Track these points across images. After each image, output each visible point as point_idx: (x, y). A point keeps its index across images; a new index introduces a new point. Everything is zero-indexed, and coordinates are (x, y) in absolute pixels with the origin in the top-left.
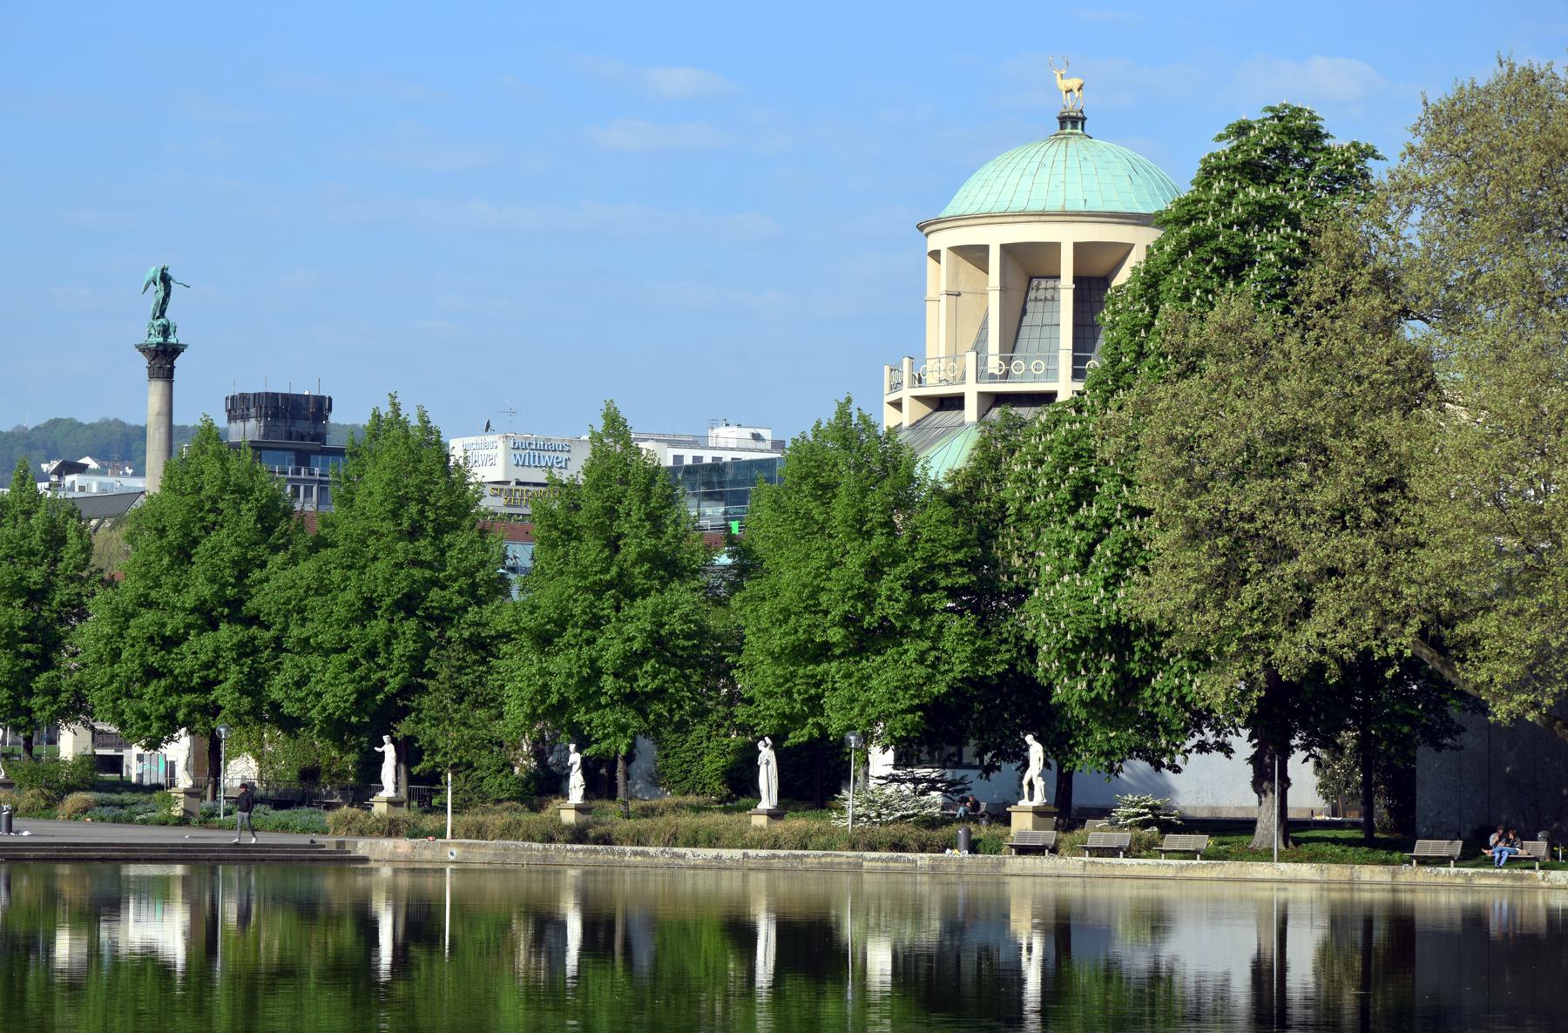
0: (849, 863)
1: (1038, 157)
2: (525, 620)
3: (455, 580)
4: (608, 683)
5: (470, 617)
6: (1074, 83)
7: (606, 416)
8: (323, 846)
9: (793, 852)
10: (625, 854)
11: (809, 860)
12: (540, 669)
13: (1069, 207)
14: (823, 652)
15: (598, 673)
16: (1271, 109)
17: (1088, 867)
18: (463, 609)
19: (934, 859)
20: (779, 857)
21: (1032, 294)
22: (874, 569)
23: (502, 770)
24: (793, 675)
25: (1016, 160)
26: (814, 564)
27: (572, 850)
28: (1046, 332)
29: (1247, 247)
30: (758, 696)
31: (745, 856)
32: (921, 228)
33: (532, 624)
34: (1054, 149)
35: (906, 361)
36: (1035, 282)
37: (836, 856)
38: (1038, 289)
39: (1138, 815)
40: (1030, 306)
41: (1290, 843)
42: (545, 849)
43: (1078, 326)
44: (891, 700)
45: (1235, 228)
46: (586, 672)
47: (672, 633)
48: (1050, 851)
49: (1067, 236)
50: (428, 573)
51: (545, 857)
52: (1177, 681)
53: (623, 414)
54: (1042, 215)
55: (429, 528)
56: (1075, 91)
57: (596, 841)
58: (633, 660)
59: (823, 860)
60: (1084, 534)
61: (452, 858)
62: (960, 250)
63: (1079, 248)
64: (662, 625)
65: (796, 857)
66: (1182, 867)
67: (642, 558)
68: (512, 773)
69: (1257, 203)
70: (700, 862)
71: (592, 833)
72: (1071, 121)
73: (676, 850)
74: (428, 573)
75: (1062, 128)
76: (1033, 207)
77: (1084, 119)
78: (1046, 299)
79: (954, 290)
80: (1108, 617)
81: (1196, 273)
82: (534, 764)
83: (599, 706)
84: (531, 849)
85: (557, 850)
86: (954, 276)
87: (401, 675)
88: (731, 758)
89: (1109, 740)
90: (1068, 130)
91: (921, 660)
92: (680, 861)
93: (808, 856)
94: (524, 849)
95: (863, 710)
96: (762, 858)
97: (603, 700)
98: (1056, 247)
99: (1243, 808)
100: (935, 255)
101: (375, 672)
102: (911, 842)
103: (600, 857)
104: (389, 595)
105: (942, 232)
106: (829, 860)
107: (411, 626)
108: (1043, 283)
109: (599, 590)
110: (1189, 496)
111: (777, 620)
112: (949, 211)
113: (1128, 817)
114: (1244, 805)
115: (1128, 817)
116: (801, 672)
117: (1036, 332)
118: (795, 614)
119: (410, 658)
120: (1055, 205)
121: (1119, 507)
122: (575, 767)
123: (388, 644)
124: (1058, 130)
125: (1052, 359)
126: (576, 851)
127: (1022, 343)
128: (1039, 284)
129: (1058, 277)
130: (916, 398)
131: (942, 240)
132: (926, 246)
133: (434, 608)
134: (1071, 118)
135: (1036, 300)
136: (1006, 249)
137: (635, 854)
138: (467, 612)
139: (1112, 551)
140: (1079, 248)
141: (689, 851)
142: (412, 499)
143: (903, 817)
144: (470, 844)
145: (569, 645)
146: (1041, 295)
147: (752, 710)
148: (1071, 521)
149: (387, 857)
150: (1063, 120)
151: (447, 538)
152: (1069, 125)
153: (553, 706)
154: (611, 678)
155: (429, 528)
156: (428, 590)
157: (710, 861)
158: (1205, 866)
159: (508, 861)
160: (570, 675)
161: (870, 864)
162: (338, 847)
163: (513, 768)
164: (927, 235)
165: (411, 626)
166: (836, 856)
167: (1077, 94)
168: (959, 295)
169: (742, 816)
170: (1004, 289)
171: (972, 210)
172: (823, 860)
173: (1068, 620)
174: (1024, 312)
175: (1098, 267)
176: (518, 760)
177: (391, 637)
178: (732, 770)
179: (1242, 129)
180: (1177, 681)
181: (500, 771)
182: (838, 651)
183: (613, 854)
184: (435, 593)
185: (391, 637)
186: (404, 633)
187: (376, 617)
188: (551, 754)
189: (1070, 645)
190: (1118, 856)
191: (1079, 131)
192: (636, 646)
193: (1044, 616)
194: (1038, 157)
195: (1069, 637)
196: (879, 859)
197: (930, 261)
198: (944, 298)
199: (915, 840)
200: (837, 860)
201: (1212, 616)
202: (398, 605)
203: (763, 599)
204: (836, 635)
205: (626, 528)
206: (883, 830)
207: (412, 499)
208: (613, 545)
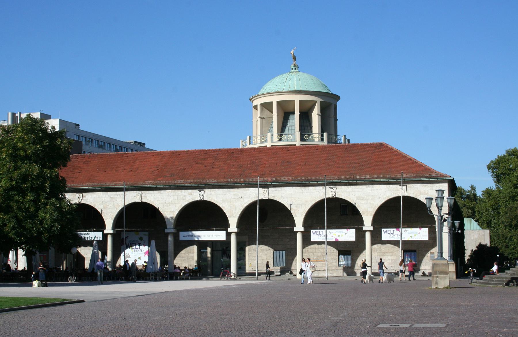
54: (289, 92)
62: (263, 105)
100: (256, 107)
112: (261, 92)
131: (258, 102)
136: (278, 103)
197: (254, 110)
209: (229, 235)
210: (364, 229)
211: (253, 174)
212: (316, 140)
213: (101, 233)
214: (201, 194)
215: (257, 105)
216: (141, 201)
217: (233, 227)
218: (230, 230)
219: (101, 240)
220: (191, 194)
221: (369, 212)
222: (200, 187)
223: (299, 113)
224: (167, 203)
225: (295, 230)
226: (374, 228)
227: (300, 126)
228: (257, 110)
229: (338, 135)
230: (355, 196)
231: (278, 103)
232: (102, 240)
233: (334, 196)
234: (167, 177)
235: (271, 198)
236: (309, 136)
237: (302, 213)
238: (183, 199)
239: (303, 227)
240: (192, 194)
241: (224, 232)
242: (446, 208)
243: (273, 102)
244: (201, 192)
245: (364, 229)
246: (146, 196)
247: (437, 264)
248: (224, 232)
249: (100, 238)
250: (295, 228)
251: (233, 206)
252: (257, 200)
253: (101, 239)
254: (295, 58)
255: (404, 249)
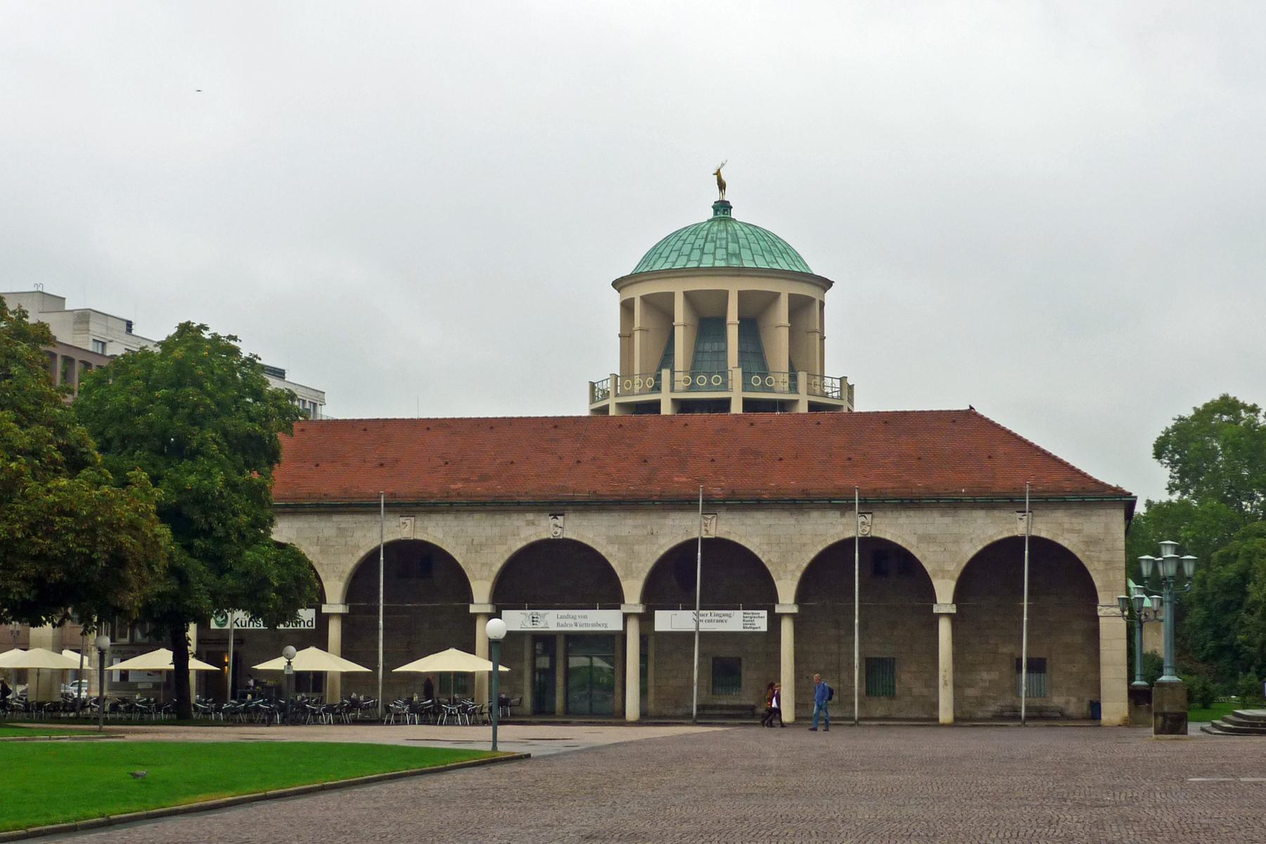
136: (687, 295)
209: (775, 620)
210: (935, 611)
211: (676, 479)
213: (313, 611)
214: (558, 524)
215: (634, 298)
216: (412, 539)
217: (787, 601)
218: (778, 610)
219: (311, 628)
220: (533, 524)
221: (949, 571)
222: (556, 507)
223: (738, 322)
224: (474, 543)
225: (471, 611)
226: (958, 609)
229: (825, 375)
230: (915, 534)
231: (642, 298)
232: (314, 627)
233: (867, 534)
234: (472, 481)
235: (722, 536)
237: (794, 571)
238: (515, 535)
239: (795, 603)
240: (536, 522)
241: (764, 613)
242: (1121, 565)
244: (557, 519)
245: (935, 611)
246: (425, 525)
248: (764, 613)
249: (310, 624)
250: (776, 606)
251: (633, 552)
252: (697, 539)
253: (312, 626)
254: (722, 186)
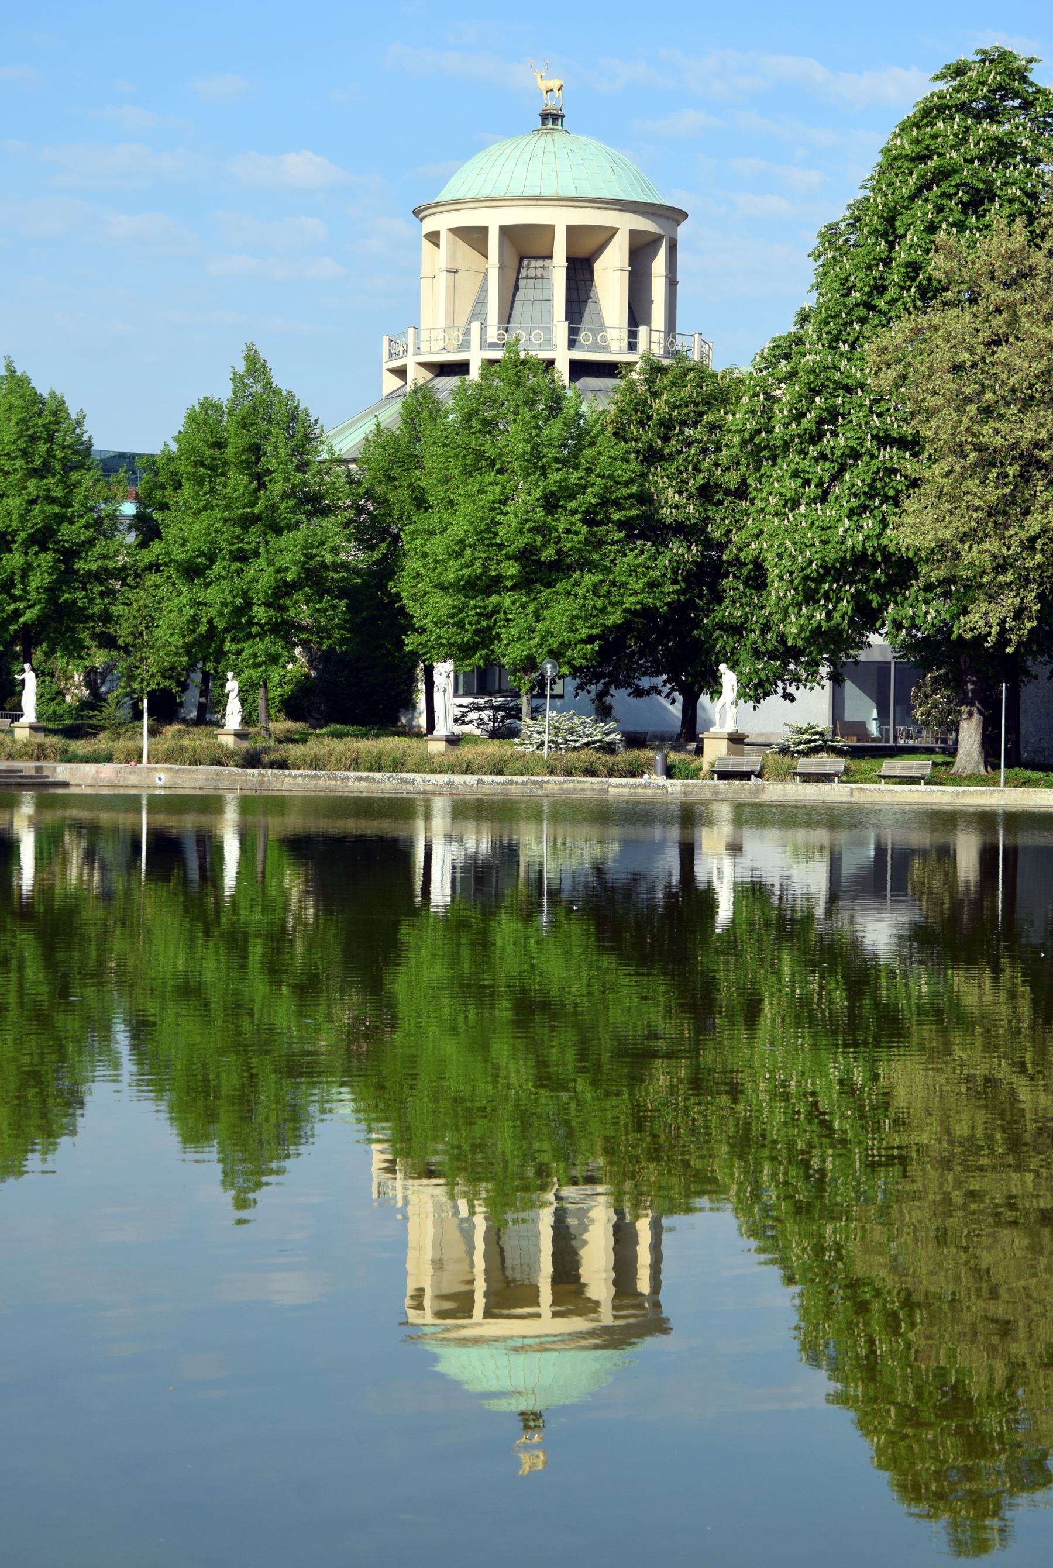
0: (593, 790)
1: (529, 148)
2: (175, 552)
3: (82, 516)
4: (260, 613)
5: (97, 550)
6: (555, 84)
7: (247, 358)
8: (21, 771)
9: (532, 778)
10: (348, 780)
11: (549, 786)
12: (191, 600)
13: (562, 193)
14: (493, 585)
15: (248, 604)
16: (984, 52)
17: (856, 793)
18: (91, 542)
19: (686, 786)
20: (517, 783)
21: (523, 273)
22: (551, 503)
23: (55, 699)
24: (465, 605)
25: (509, 150)
26: (490, 497)
27: (290, 775)
28: (538, 306)
29: (989, 183)
30: (430, 626)
31: (479, 781)
32: (417, 213)
33: (184, 556)
34: (541, 142)
35: (411, 331)
36: (525, 262)
37: (578, 782)
38: (528, 268)
39: (810, 741)
40: (522, 283)
41: (989, 769)
42: (260, 774)
43: (569, 301)
44: (571, 631)
45: (976, 163)
46: (239, 601)
47: (323, 564)
48: (756, 776)
49: (560, 219)
50: (57, 509)
51: (261, 783)
52: (911, 611)
53: (263, 355)
54: (539, 200)
55: (58, 466)
56: (556, 90)
57: (272, 765)
58: (283, 590)
59: (565, 786)
60: (827, 465)
61: (160, 783)
62: (460, 232)
63: (571, 230)
64: (311, 557)
65: (535, 783)
66: (958, 794)
67: (285, 496)
68: (64, 701)
69: (996, 138)
70: (430, 788)
71: (266, 759)
72: (552, 118)
73: (404, 775)
74: (57, 509)
75: (543, 124)
76: (529, 192)
77: (563, 116)
78: (536, 277)
79: (452, 267)
80: (853, 548)
81: (940, 209)
82: (86, 692)
83: (250, 636)
84: (246, 775)
85: (230, 774)
86: (452, 256)
87: (39, 607)
88: (287, 688)
89: (757, 671)
90: (550, 126)
91: (595, 590)
92: (409, 787)
93: (548, 782)
94: (237, 774)
95: (543, 638)
96: (498, 784)
97: (254, 630)
98: (550, 229)
99: (763, 734)
100: (433, 237)
101: (9, 605)
102: (601, 768)
103: (321, 782)
104: (23, 530)
105: (441, 215)
106: (571, 786)
107: (47, 559)
108: (533, 263)
109: (247, 522)
110: (982, 422)
111: (454, 551)
112: (444, 196)
113: (800, 743)
114: (764, 731)
115: (800, 743)
116: (472, 603)
117: (528, 306)
118: (470, 546)
119: (47, 590)
120: (550, 192)
121: (869, 437)
122: (232, 695)
123: (24, 576)
124: (540, 126)
125: (548, 329)
126: (295, 777)
127: (515, 316)
128: (529, 263)
129: (550, 257)
130: (420, 364)
131: (441, 222)
132: (420, 229)
133: (66, 541)
134: (552, 115)
135: (527, 277)
136: (505, 230)
137: (360, 779)
138: (95, 546)
139: (863, 481)
140: (571, 230)
141: (418, 777)
142: (40, 438)
143: (588, 744)
144: (179, 770)
145: (219, 578)
146: (532, 273)
147: (422, 638)
148: (813, 451)
149: (89, 782)
150: (545, 117)
151: (74, 476)
152: (551, 122)
153: (201, 635)
154: (263, 609)
155: (58, 466)
156: (59, 524)
157: (441, 786)
158: (984, 792)
159: (221, 786)
160: (224, 604)
161: (616, 790)
162: (37, 772)
163: (64, 696)
164: (422, 220)
165: (47, 559)
166: (578, 782)
167: (557, 94)
168: (456, 272)
169: (421, 744)
170: (501, 268)
171: (471, 195)
172: (565, 786)
173: (814, 549)
174: (516, 289)
175: (584, 249)
176: (69, 689)
177: (26, 570)
178: (290, 698)
179: (960, 70)
180: (911, 611)
181: (52, 700)
182: (509, 584)
183: (335, 779)
184: (65, 528)
185: (26, 570)
186: (39, 566)
187: (10, 551)
188: (103, 683)
189: (814, 575)
190: (919, 784)
191: (559, 127)
192: (290, 577)
193: (789, 544)
194: (529, 148)
195: (814, 566)
196: (626, 785)
197: (426, 244)
198: (443, 276)
199: (604, 765)
200: (580, 786)
201: (992, 545)
202: (32, 540)
203: (432, 533)
204: (512, 569)
205: (273, 465)
206: (573, 755)
207: (40, 438)
208: (260, 480)
212: (615, 346)
227: (567, 301)
228: (438, 246)
231: (505, 230)
236: (594, 336)
243: (631, 231)
247: (243, 966)
255: (630, 728)
